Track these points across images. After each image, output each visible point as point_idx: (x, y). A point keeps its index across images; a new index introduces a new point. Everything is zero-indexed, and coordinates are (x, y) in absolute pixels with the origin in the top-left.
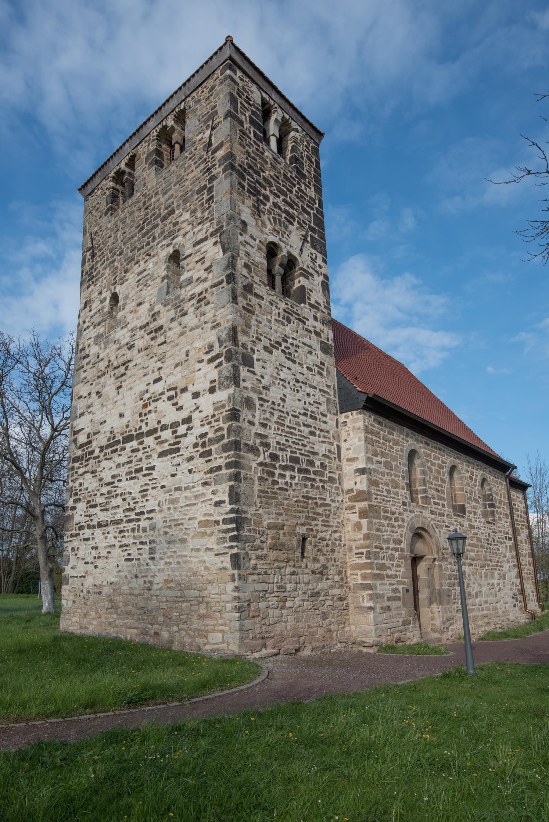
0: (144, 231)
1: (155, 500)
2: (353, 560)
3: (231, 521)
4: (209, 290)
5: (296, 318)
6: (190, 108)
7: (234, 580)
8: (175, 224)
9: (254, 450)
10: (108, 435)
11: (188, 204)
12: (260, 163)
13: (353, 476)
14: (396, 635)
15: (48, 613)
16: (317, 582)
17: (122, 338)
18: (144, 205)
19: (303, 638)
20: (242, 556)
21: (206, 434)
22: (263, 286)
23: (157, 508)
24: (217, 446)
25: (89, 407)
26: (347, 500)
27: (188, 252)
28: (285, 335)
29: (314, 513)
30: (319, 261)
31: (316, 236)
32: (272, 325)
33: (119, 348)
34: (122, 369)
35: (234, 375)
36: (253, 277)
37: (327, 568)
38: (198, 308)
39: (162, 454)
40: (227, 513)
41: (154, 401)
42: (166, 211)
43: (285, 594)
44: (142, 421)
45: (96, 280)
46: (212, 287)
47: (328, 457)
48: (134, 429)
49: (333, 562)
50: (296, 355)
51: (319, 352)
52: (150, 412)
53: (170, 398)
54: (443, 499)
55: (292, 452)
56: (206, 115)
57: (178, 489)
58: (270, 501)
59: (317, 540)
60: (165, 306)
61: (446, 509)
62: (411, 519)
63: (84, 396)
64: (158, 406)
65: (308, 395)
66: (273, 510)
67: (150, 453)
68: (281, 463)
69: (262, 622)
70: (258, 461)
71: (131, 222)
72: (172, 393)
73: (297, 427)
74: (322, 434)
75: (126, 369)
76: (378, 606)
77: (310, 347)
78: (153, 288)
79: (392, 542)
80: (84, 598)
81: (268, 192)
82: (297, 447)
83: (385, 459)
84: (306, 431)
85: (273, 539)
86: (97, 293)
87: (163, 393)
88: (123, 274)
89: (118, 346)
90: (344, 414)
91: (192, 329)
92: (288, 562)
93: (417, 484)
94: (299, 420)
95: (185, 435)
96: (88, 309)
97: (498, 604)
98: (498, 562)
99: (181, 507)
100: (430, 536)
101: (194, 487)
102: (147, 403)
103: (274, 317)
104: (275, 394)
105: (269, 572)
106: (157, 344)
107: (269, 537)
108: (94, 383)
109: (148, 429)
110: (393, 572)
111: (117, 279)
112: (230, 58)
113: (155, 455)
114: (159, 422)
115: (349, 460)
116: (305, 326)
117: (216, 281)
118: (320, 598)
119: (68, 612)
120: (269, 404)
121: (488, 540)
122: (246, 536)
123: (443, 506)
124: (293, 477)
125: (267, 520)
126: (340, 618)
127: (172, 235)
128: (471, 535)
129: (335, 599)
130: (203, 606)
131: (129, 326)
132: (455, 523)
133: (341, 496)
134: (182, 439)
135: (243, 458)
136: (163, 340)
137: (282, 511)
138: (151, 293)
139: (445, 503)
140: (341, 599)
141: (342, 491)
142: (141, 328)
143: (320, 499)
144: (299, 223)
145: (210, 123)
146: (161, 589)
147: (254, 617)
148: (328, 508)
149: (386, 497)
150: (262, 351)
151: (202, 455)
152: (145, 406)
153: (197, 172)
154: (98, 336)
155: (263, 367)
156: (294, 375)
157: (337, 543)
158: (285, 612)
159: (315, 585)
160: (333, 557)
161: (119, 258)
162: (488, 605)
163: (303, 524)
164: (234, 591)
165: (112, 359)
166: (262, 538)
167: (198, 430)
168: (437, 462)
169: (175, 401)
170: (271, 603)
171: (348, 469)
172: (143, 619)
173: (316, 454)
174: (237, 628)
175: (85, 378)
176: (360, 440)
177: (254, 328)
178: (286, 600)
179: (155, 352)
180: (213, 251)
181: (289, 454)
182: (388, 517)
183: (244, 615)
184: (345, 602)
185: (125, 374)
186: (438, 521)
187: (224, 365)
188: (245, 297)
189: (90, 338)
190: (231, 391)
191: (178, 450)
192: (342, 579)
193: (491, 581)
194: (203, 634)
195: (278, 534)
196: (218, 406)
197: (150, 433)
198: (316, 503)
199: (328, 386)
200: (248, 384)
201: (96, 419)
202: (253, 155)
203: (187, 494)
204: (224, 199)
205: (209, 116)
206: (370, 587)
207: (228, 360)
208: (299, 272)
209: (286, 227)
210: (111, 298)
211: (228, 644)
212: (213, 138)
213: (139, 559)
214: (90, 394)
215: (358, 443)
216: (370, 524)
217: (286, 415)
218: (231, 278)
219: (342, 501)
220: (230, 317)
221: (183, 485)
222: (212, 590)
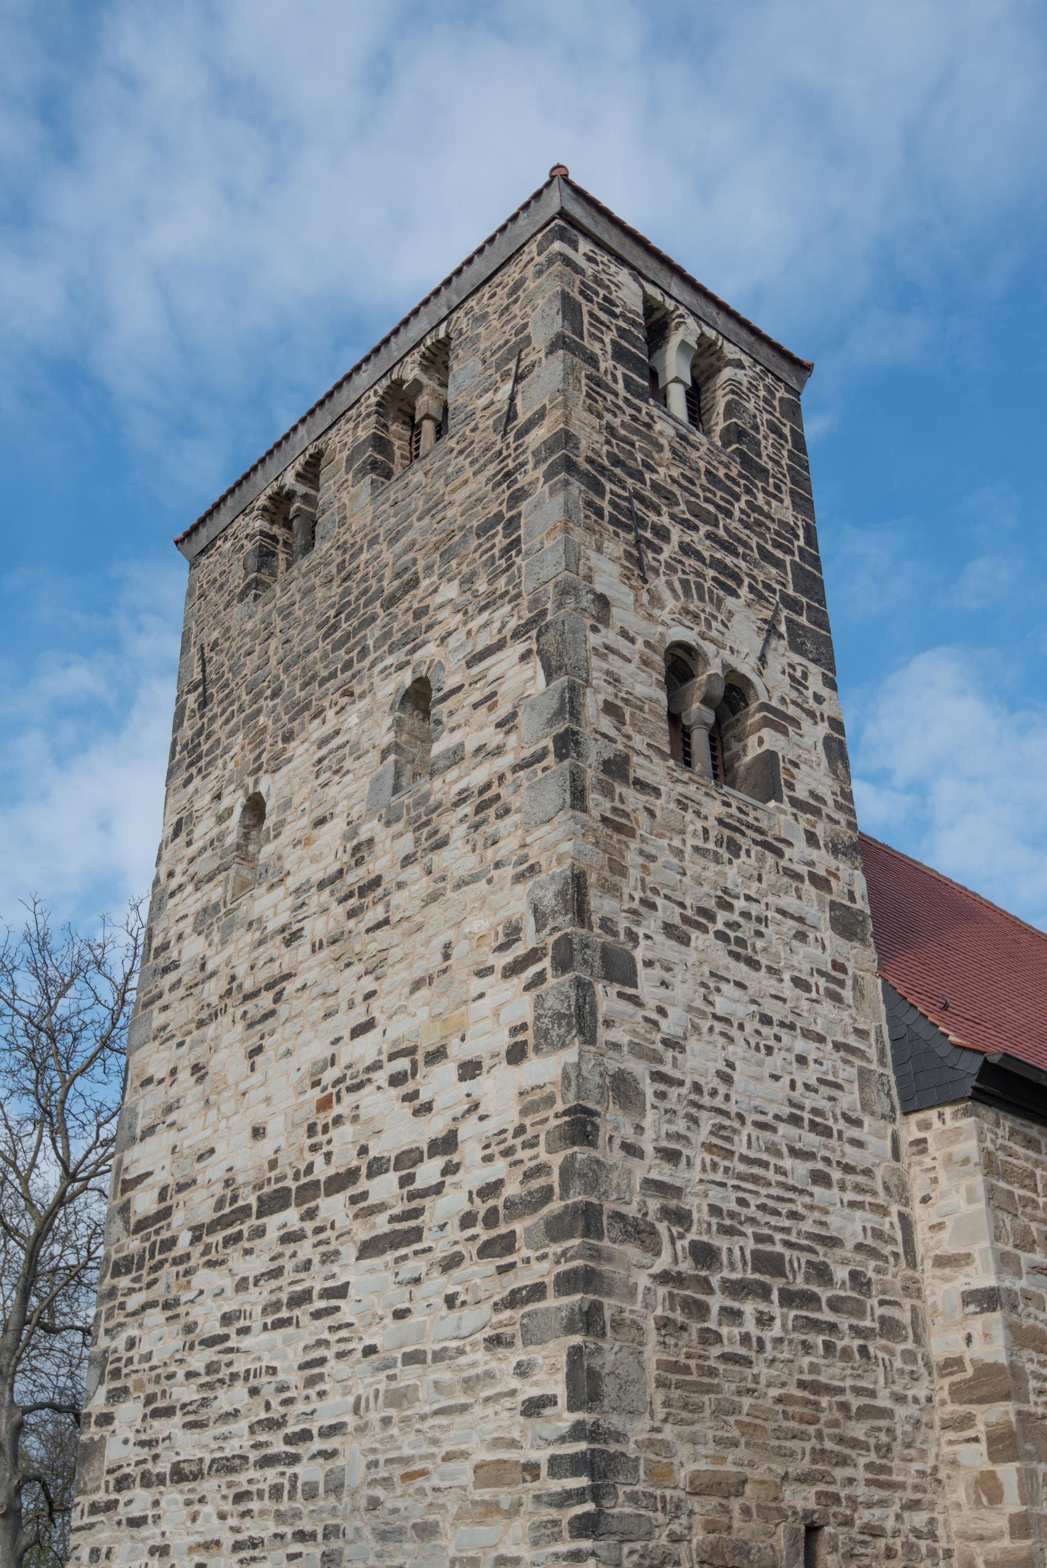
3: (576, 1465)
5: (755, 842)
9: (641, 1233)
10: (218, 1189)
13: (959, 1316)
17: (270, 913)
18: (339, 572)
21: (499, 1184)
22: (656, 759)
23: (350, 1419)
24: (529, 1221)
25: (169, 1109)
26: (945, 1394)
27: (451, 683)
28: (725, 891)
29: (841, 1440)
30: (815, 683)
31: (803, 620)
32: (687, 864)
33: (261, 942)
34: (266, 1000)
35: (579, 1008)
36: (629, 737)
38: (476, 827)
39: (369, 1249)
40: (562, 1439)
41: (349, 1089)
42: (396, 583)
44: (314, 1148)
45: (209, 764)
46: (516, 768)
48: (290, 1173)
50: (760, 944)
51: (827, 934)
52: (338, 1120)
53: (396, 1080)
55: (759, 1238)
56: (500, 347)
57: (414, 1358)
58: (695, 1398)
59: (854, 1532)
63: (158, 1077)
64: (363, 1104)
65: (802, 1060)
66: (706, 1427)
67: (334, 1245)
68: (726, 1274)
70: (657, 1269)
72: (403, 1064)
73: (773, 1161)
74: (850, 1178)
77: (801, 920)
78: (356, 779)
81: (665, 520)
82: (773, 1220)
84: (800, 1169)
85: (711, 1527)
86: (208, 798)
87: (376, 1066)
88: (280, 745)
89: (257, 935)
90: (914, 1118)
94: (775, 1138)
95: (437, 1189)
99: (423, 1418)
101: (461, 1351)
102: (331, 1093)
103: (691, 842)
104: (700, 1060)
107: (698, 1520)
109: (331, 1171)
111: (264, 757)
112: (563, 214)
113: (349, 1252)
114: (364, 1150)
115: (941, 1262)
116: (783, 863)
117: (527, 753)
120: (684, 1091)
122: (621, 1517)
124: (764, 1320)
125: (690, 1463)
134: (427, 1202)
135: (610, 1259)
137: (735, 1433)
138: (352, 791)
141: (927, 1365)
142: (321, 885)
143: (857, 1391)
144: (752, 589)
145: (512, 365)
148: (883, 1423)
150: (660, 938)
151: (486, 1250)
152: (324, 1104)
153: (478, 485)
155: (663, 983)
156: (754, 1002)
157: (923, 1544)
163: (804, 1479)
165: (241, 971)
166: (675, 1527)
167: (475, 1174)
169: (409, 1087)
171: (942, 1291)
173: (834, 1242)
175: (164, 1028)
176: (971, 1199)
177: (634, 874)
179: (357, 949)
180: (520, 677)
181: (750, 1245)
185: (272, 1013)
187: (551, 981)
188: (607, 792)
189: (185, 917)
190: (570, 1055)
191: (417, 1234)
195: (726, 1510)
196: (533, 1102)
198: (844, 1407)
199: (861, 1033)
200: (619, 1035)
202: (623, 432)
203: (442, 1373)
205: (510, 350)
207: (562, 965)
208: (759, 716)
210: (245, 809)
212: (518, 401)
214: (174, 1072)
215: (965, 1208)
216: (1027, 1478)
217: (736, 1124)
218: (567, 744)
219: (929, 1399)
220: (567, 847)
221: (430, 1347)
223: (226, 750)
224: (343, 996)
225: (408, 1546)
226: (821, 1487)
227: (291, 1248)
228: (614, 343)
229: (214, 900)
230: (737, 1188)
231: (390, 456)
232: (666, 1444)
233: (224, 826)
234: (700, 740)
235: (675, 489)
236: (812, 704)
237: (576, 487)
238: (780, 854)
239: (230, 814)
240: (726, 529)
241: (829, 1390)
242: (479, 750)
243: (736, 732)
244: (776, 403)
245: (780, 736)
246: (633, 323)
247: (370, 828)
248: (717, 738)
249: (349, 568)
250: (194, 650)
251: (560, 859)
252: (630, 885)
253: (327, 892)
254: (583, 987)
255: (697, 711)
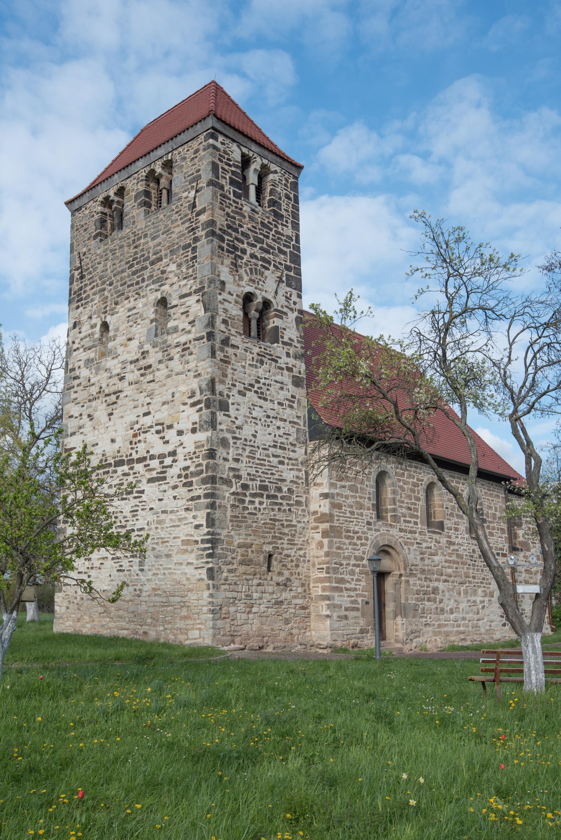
0: (134, 269)
1: (145, 519)
2: (316, 574)
3: (208, 541)
4: (193, 342)
5: (269, 359)
6: (176, 162)
7: (209, 589)
8: (163, 272)
9: (228, 482)
10: (100, 457)
11: (175, 256)
12: (238, 219)
14: (352, 641)
15: (33, 621)
16: (281, 593)
17: (113, 368)
18: (133, 243)
19: (267, 638)
20: (216, 570)
21: (189, 467)
22: (238, 336)
23: (146, 527)
24: (197, 478)
25: (80, 428)
26: (312, 520)
27: (174, 303)
28: (258, 377)
29: (281, 533)
30: (294, 298)
31: (292, 274)
32: (246, 370)
33: (110, 377)
34: (113, 398)
35: (212, 420)
36: (230, 330)
37: (290, 581)
38: (182, 356)
39: (150, 481)
40: (205, 535)
41: (143, 432)
42: (154, 257)
43: (252, 601)
44: (132, 448)
45: (86, 303)
46: (195, 340)
47: (295, 483)
48: (125, 455)
49: (297, 576)
50: (268, 393)
51: (290, 387)
52: (139, 441)
53: (158, 432)
54: (417, 517)
55: (261, 481)
56: (191, 175)
57: (164, 512)
58: (240, 524)
59: (282, 556)
60: (153, 347)
61: (419, 526)
62: (376, 537)
63: (75, 416)
64: (148, 438)
65: (279, 428)
66: (243, 531)
67: (139, 478)
68: (251, 491)
69: (232, 623)
70: (231, 491)
71: (121, 255)
72: (160, 428)
73: (267, 459)
74: (291, 462)
75: (118, 398)
76: (335, 615)
77: (282, 383)
78: (142, 328)
79: (353, 558)
80: (78, 604)
81: (245, 246)
82: (266, 476)
83: (350, 483)
84: (275, 461)
85: (242, 555)
86: (86, 317)
87: (151, 427)
88: (114, 306)
89: (109, 374)
91: (177, 374)
92: (254, 575)
93: (388, 502)
94: (268, 452)
95: (171, 466)
96: (77, 330)
97: (480, 623)
98: (484, 579)
99: (167, 528)
100: (397, 553)
101: (178, 511)
102: (137, 434)
103: (248, 362)
104: (247, 432)
105: (238, 583)
106: (146, 381)
107: (239, 554)
108: (86, 405)
109: (138, 456)
110: (353, 586)
111: (108, 308)
113: (144, 481)
114: (148, 452)
116: (278, 365)
117: (198, 335)
118: (283, 607)
119: (61, 618)
120: (242, 441)
121: (472, 556)
122: (219, 553)
123: (416, 523)
124: (261, 503)
125: (238, 540)
126: (301, 624)
127: (160, 281)
128: (450, 551)
129: (297, 607)
130: (184, 609)
131: (119, 357)
132: (429, 540)
133: (308, 517)
134: (168, 469)
135: (218, 490)
136: (152, 379)
137: (251, 532)
138: (141, 331)
139: (419, 521)
140: (303, 608)
141: (308, 513)
142: (131, 362)
143: (287, 520)
144: (274, 266)
145: (195, 184)
146: (149, 596)
147: (224, 618)
148: (293, 529)
149: (350, 518)
150: (237, 395)
151: (185, 485)
152: (135, 436)
153: (182, 228)
154: (88, 360)
155: (237, 410)
156: (265, 412)
157: (302, 559)
158: (251, 616)
159: (279, 595)
160: (297, 571)
161: (110, 288)
162: (467, 622)
163: (269, 543)
164: (209, 597)
165: (104, 386)
166: (233, 555)
167: (181, 464)
168: (411, 480)
169: (162, 435)
170: (239, 608)
172: (134, 622)
173: (284, 480)
174: (211, 626)
175: (76, 399)
177: (230, 376)
178: (253, 607)
179: (144, 388)
180: (197, 309)
181: (259, 483)
182: (350, 536)
183: (217, 616)
184: (307, 611)
185: (116, 403)
186: (408, 538)
187: (204, 411)
188: (222, 350)
189: (80, 360)
190: (209, 434)
191: (165, 478)
192: (305, 591)
193: (473, 598)
194: (185, 631)
195: (247, 551)
196: (199, 446)
197: (140, 460)
198: (282, 525)
199: (298, 417)
200: (223, 427)
201: (88, 440)
202: (232, 214)
203: (172, 516)
204: (206, 262)
205: (194, 178)
206: (328, 598)
207: (208, 406)
208: (274, 313)
209: (262, 274)
210: (101, 326)
211: (204, 639)
212: (197, 200)
213: (130, 570)
214: (81, 415)
216: (330, 542)
217: (257, 449)
218: (210, 336)
219: (308, 522)
220: (209, 370)
221: (169, 509)
222: (192, 596)
223: (92, 300)
224: (140, 402)
225: (163, 560)
226: (274, 545)
227: (125, 478)
228: (230, 178)
229: (91, 357)
230: (256, 467)
231: (150, 198)
232: (232, 536)
233: (94, 330)
234: (254, 323)
235: (250, 233)
236: (292, 306)
237: (216, 241)
238: (276, 362)
239: (96, 326)
240: (267, 244)
241: (278, 520)
242: (183, 330)
243: (267, 316)
244: (289, 185)
245: (280, 320)
246: (237, 167)
247: (147, 347)
248: (260, 321)
249: (137, 243)
250: (76, 253)
251: (207, 373)
252: (228, 381)
253: (133, 365)
254: (213, 414)
255: (254, 314)
